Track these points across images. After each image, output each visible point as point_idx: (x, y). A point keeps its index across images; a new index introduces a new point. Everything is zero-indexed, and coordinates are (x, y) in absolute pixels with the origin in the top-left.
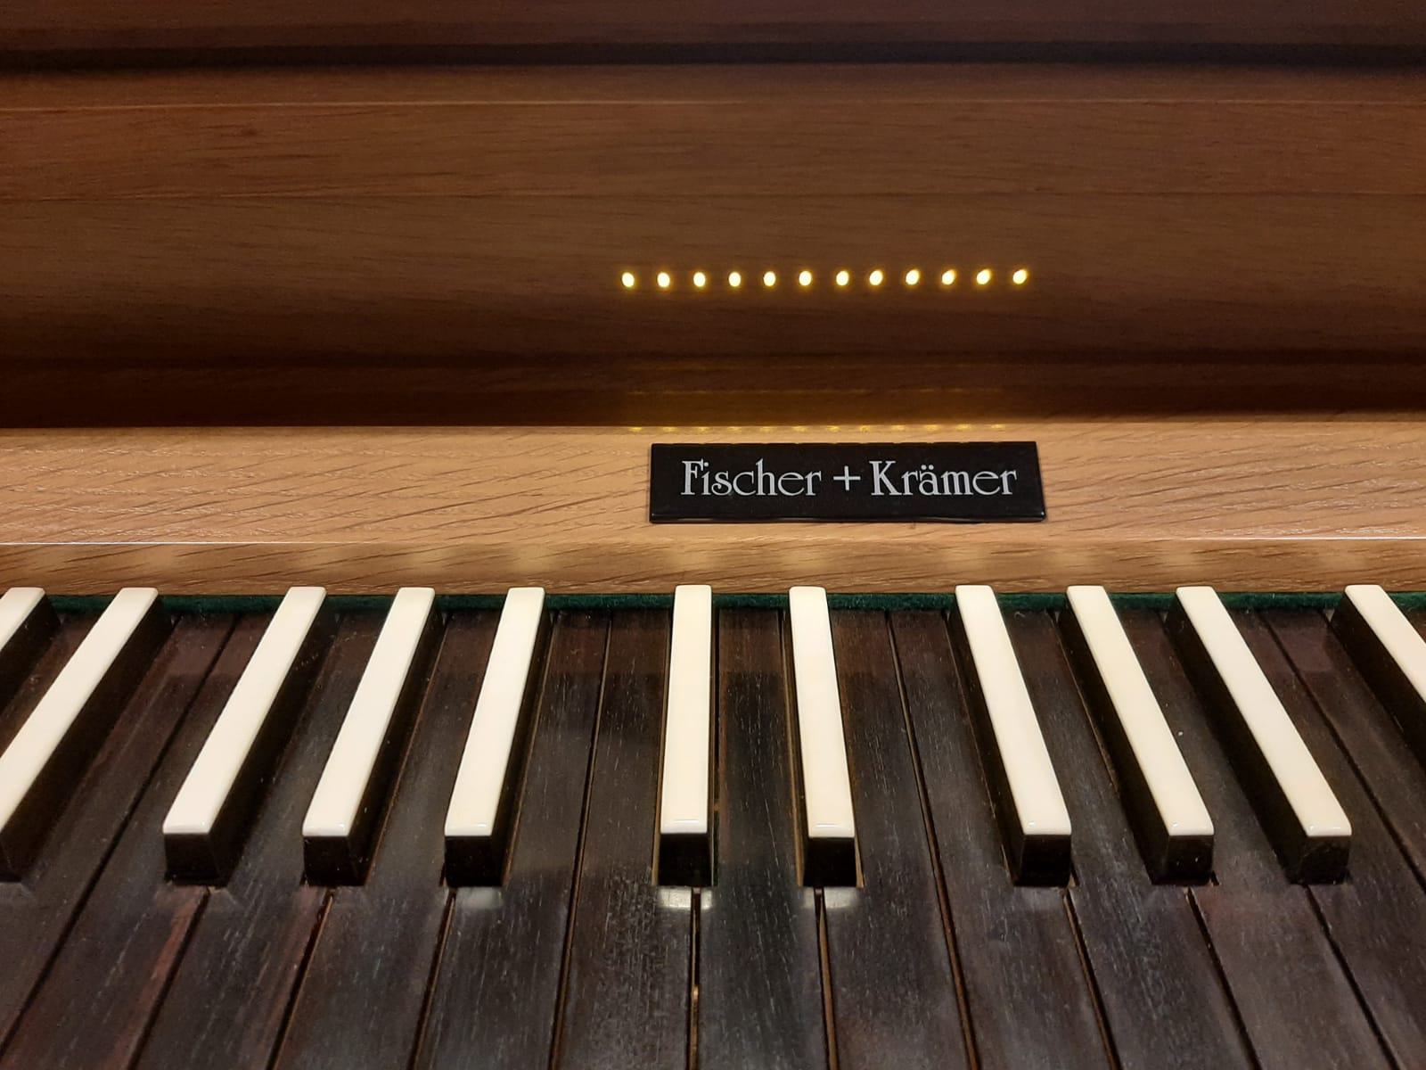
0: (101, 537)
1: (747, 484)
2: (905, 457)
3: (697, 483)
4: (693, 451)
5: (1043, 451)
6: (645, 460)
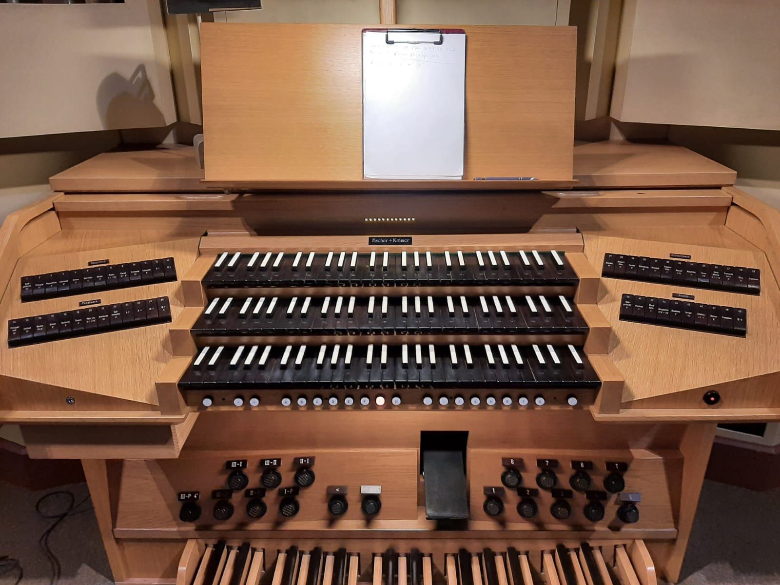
0: (309, 246)
4: (395, 238)
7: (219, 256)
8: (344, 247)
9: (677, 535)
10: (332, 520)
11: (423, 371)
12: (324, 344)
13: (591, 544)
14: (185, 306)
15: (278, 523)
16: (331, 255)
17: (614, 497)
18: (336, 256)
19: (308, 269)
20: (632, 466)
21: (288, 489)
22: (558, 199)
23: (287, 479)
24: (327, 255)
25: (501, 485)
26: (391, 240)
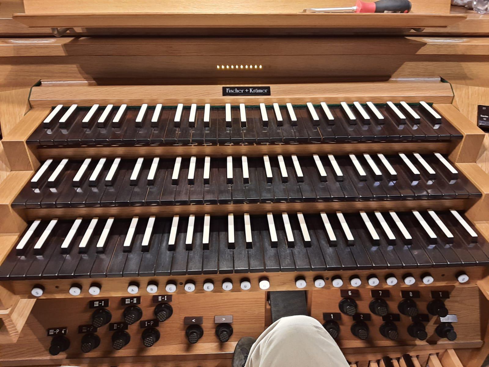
0: (155, 97)
1: (234, 91)
2: (254, 88)
3: (228, 91)
4: (228, 87)
5: (271, 88)
6: (222, 89)
7: (53, 108)
8: (195, 98)
9: (483, 346)
10: (190, 343)
11: (296, 250)
12: (176, 214)
13: (411, 354)
14: (11, 171)
15: (142, 348)
16: (180, 108)
17: (434, 318)
18: (187, 109)
19: (155, 125)
20: (453, 293)
21: (149, 321)
22: (424, 44)
23: (148, 313)
24: (176, 108)
25: (338, 311)
26: (247, 90)
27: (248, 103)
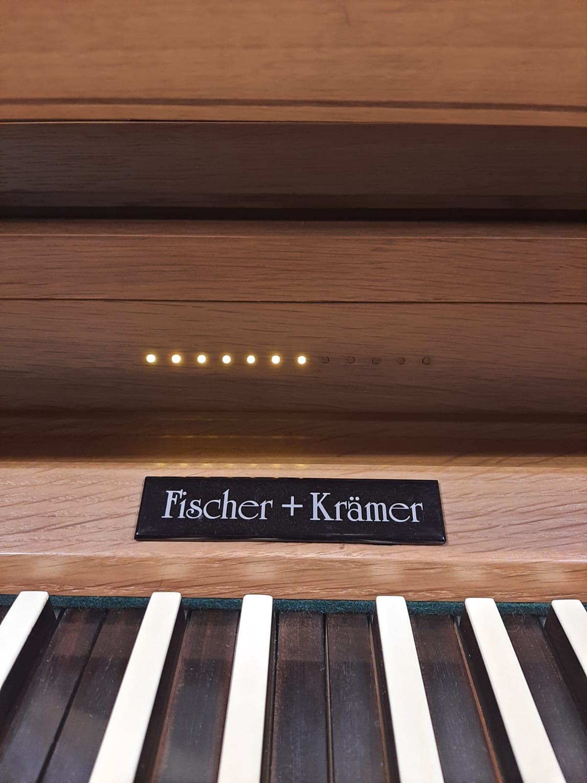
1: (214, 510)
3: (175, 509)
5: (443, 488)
27: (300, 589)
